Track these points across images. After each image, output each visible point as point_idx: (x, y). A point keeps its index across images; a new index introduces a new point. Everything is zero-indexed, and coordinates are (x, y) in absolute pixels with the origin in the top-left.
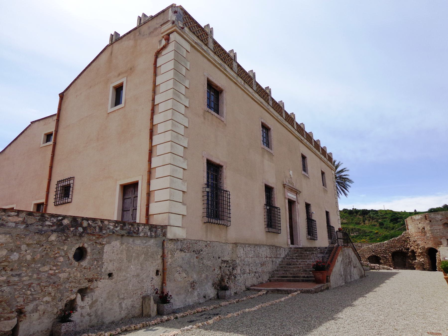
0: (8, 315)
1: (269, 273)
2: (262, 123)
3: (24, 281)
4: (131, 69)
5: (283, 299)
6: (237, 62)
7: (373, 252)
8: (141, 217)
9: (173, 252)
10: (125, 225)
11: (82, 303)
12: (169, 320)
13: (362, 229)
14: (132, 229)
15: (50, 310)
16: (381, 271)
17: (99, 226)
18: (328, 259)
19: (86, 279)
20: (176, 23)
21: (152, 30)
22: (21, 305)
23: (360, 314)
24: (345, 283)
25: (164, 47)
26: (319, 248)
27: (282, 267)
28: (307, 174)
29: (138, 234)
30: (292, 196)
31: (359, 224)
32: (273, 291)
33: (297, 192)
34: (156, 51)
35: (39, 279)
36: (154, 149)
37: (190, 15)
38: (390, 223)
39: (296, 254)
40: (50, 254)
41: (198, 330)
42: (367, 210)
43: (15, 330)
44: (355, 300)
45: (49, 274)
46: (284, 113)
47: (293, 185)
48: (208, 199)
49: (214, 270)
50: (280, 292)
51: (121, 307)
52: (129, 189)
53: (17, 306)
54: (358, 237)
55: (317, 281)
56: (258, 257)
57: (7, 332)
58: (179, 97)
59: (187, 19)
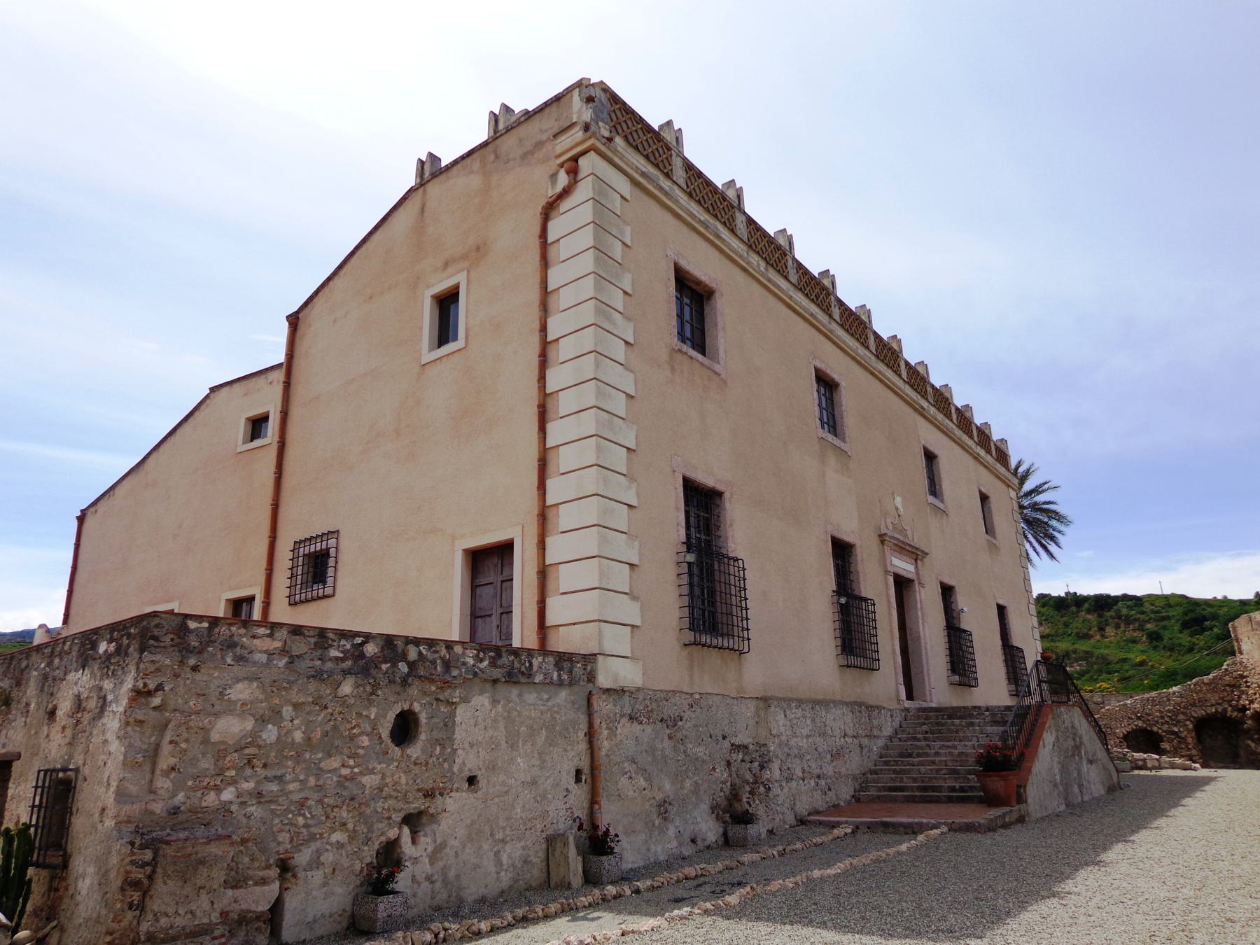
0: (261, 874)
1: (855, 778)
2: (817, 370)
3: (291, 792)
4: (478, 249)
5: (904, 847)
6: (745, 213)
7: (1139, 718)
8: (525, 633)
9: (612, 722)
10: (499, 655)
11: (413, 849)
12: (620, 896)
13: (1097, 652)
14: (517, 665)
15: (346, 865)
16: (1164, 773)
17: (442, 659)
18: (1018, 738)
19: (419, 790)
20: (593, 128)
21: (528, 146)
22: (287, 851)
23: (1125, 884)
24: (1067, 806)
25: (566, 192)
26: (988, 709)
27: (887, 763)
28: (942, 501)
29: (529, 676)
30: (904, 566)
31: (1087, 637)
32: (871, 827)
33: (916, 555)
34: (543, 202)
35: (319, 788)
36: (551, 456)
37: (624, 103)
38: (1181, 632)
39: (924, 727)
40: (342, 728)
41: (708, 920)
42: (1108, 596)
43: (277, 908)
44: (1105, 849)
45: (340, 776)
46: (872, 338)
47: (906, 536)
48: (691, 585)
49: (714, 769)
50: (891, 830)
51: (499, 863)
52: (488, 561)
53: (278, 852)
54: (1087, 677)
55: (991, 800)
56: (823, 735)
57: (262, 912)
58: (609, 319)
59: (618, 113)
